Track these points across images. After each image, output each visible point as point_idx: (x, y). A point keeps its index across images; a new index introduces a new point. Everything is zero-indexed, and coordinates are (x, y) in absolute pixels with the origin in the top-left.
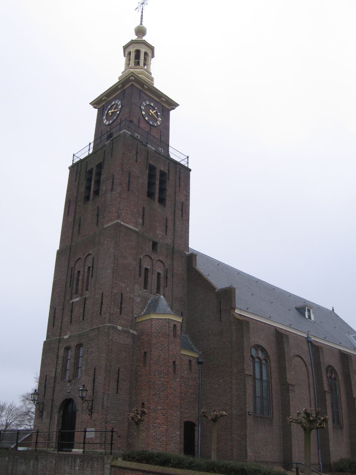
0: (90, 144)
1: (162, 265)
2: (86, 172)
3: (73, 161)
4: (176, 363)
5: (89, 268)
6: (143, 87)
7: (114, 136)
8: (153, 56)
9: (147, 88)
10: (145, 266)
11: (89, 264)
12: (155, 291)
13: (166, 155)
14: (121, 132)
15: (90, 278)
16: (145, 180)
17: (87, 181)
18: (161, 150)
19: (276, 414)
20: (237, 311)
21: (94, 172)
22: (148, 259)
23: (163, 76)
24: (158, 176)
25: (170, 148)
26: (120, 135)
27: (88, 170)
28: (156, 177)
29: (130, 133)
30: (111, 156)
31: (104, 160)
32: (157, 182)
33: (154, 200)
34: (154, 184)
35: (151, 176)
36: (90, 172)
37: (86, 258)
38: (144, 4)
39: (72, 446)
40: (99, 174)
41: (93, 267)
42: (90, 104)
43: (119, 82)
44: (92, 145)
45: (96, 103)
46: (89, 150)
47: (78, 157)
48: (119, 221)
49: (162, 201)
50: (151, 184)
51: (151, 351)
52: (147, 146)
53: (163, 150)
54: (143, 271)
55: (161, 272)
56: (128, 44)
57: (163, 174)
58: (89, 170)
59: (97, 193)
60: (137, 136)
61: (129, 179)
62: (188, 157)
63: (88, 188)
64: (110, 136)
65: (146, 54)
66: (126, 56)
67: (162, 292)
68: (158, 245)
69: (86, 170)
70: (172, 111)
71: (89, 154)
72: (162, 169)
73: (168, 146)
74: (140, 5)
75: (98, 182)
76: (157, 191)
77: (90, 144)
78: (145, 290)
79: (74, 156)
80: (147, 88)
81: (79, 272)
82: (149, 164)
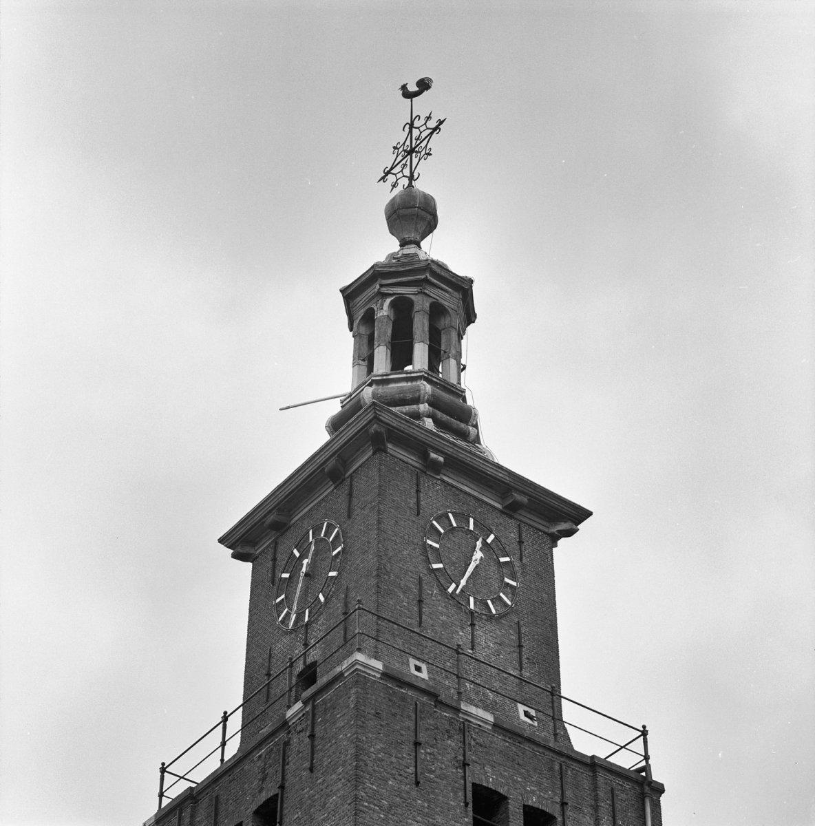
0: (225, 718)
3: (161, 795)
6: (424, 456)
7: (322, 680)
8: (470, 317)
9: (441, 459)
13: (545, 735)
14: (345, 665)
18: (418, 669)
23: (522, 402)
26: (341, 674)
28: (507, 809)
29: (379, 665)
30: (311, 770)
31: (282, 787)
38: (417, 152)
42: (222, 541)
43: (327, 444)
44: (235, 723)
45: (243, 540)
46: (223, 744)
47: (182, 775)
52: (457, 710)
56: (364, 278)
60: (418, 669)
62: (644, 733)
64: (309, 676)
65: (437, 311)
71: (222, 760)
72: (533, 801)
74: (400, 158)
77: (225, 718)
79: (166, 774)
80: (441, 459)
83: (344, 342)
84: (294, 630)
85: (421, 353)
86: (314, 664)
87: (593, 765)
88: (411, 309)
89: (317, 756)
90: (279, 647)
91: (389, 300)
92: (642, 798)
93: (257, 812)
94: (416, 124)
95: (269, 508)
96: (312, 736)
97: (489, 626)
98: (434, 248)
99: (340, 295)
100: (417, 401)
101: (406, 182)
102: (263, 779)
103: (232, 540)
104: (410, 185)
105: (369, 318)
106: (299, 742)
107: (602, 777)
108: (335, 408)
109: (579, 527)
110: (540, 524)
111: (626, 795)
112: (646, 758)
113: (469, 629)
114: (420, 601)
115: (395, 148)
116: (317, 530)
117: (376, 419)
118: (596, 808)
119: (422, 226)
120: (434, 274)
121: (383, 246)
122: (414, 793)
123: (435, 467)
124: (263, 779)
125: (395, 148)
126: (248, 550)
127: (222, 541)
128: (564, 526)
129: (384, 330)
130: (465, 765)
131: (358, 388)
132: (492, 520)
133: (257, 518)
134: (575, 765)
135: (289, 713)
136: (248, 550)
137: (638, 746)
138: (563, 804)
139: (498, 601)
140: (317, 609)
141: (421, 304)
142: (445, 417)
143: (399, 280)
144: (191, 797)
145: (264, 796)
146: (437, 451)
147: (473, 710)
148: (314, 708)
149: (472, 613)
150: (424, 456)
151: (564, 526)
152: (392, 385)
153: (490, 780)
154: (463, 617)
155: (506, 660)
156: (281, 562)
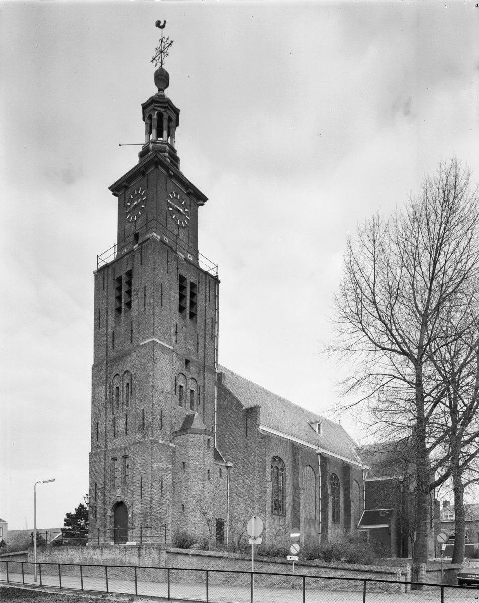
0: (115, 246)
1: (195, 384)
4: (210, 471)
5: (128, 384)
8: (177, 124)
10: (179, 384)
13: (194, 263)
18: (166, 239)
19: (289, 512)
20: (261, 427)
22: (182, 377)
24: (188, 287)
25: (199, 255)
27: (116, 278)
31: (133, 268)
32: (188, 297)
36: (119, 280)
37: (123, 375)
39: (127, 540)
40: (129, 283)
42: (109, 188)
45: (117, 189)
46: (115, 253)
48: (154, 339)
49: (193, 315)
51: (189, 461)
52: (177, 253)
53: (167, 240)
54: (178, 389)
55: (194, 390)
57: (193, 286)
59: (129, 304)
62: (217, 267)
66: (146, 119)
67: (195, 409)
74: (158, 54)
75: (129, 293)
76: (188, 305)
77: (115, 246)
81: (118, 388)
83: (142, 126)
84: (132, 221)
85: (165, 133)
86: (138, 233)
87: (206, 273)
88: (161, 115)
89: (143, 261)
90: (127, 226)
91: (156, 112)
92: (216, 283)
93: (126, 274)
94: (164, 40)
95: (123, 181)
96: (141, 255)
97: (182, 230)
98: (169, 93)
99: (141, 107)
100: (164, 152)
101: (159, 64)
102: (127, 265)
103: (113, 188)
104: (161, 67)
105: (150, 117)
106: (137, 256)
107: (207, 277)
108: (140, 149)
109: (205, 203)
110: (195, 200)
111: (212, 282)
112: (217, 273)
113: (177, 230)
114: (167, 219)
115: (168, 55)
116: (138, 191)
117: (156, 156)
118: (206, 285)
119: (165, 84)
120: (170, 105)
121: (154, 91)
122: (167, 275)
123: (170, 176)
124: (127, 265)
125: (168, 55)
126: (116, 193)
127: (109, 188)
128: (201, 202)
129: (155, 123)
130: (178, 269)
131: (148, 143)
132: (185, 197)
133: (120, 183)
134: (202, 273)
135: (134, 247)
136: (116, 193)
137: (215, 269)
138: (199, 283)
139: (185, 222)
140: (139, 216)
141: (166, 116)
142: (172, 159)
143: (163, 105)
144: (106, 266)
145: (128, 269)
146: (172, 171)
147: (180, 254)
148: (141, 246)
149: (178, 225)
150: (168, 172)
151: (201, 202)
152: (158, 144)
153: (183, 274)
154: (177, 226)
155: (186, 240)
156: (127, 199)
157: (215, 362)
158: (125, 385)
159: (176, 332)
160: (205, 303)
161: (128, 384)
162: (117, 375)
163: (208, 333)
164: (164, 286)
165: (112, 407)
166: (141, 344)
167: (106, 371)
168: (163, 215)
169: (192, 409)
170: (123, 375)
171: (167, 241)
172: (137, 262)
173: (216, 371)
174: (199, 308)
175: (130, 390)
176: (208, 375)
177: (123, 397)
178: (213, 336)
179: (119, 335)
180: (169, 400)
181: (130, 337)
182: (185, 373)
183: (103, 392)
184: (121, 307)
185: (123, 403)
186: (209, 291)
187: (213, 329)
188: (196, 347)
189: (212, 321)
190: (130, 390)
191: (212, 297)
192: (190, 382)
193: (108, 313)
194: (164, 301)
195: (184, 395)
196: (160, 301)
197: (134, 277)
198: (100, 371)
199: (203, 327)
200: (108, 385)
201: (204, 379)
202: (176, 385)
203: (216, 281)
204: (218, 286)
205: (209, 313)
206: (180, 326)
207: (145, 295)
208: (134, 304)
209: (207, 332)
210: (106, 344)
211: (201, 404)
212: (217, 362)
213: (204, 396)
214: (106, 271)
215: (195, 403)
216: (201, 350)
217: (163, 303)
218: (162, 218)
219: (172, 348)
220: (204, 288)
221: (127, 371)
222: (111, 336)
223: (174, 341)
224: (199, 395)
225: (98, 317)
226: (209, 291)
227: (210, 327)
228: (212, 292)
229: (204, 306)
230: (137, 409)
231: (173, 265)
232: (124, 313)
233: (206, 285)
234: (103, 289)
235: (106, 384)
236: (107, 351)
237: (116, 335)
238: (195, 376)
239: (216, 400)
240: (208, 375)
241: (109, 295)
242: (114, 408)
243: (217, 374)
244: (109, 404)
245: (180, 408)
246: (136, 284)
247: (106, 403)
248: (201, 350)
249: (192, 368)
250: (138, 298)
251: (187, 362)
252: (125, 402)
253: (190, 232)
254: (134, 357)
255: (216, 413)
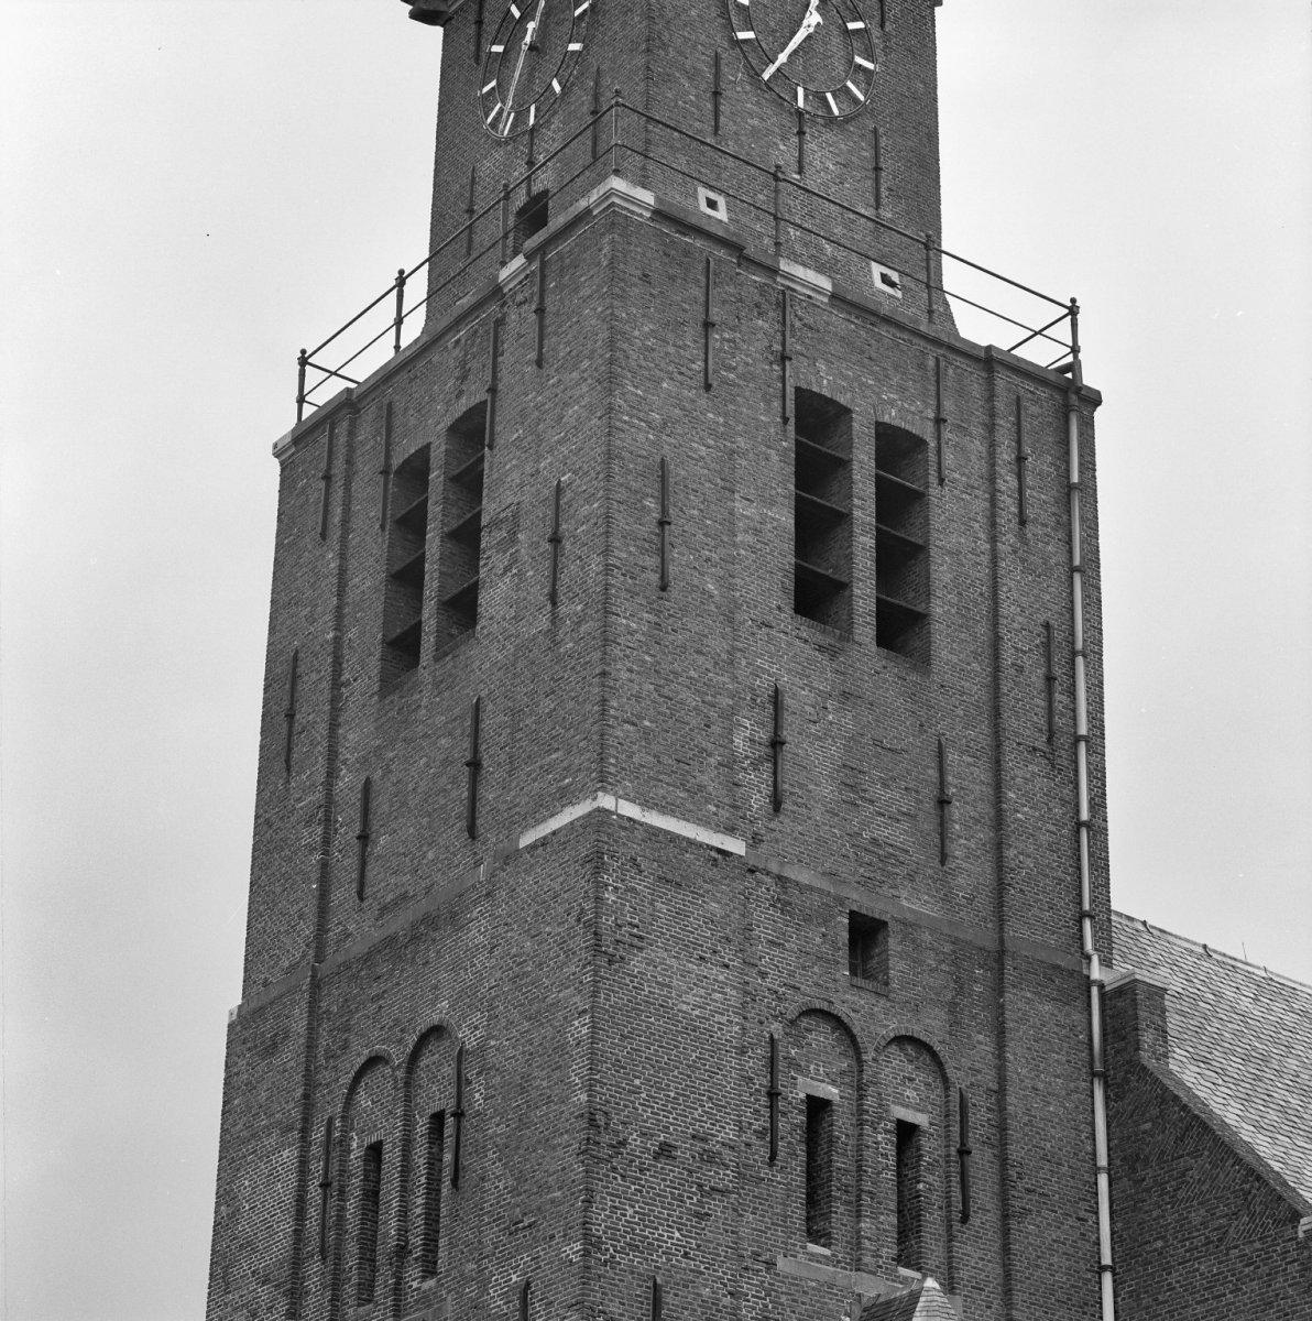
0: (401, 281)
2: (385, 472)
3: (301, 400)
5: (438, 1118)
7: (557, 221)
10: (804, 1087)
11: (435, 1096)
12: (889, 1251)
13: (913, 313)
15: (446, 1190)
16: (767, 515)
17: (395, 521)
21: (436, 476)
22: (821, 1036)
24: (863, 461)
26: (588, 211)
27: (396, 462)
29: (647, 197)
30: (539, 363)
31: (493, 390)
32: (864, 511)
33: (847, 634)
34: (842, 519)
35: (816, 468)
36: (415, 471)
37: (414, 1057)
40: (469, 483)
41: (459, 1115)
44: (417, 288)
46: (399, 321)
47: (333, 370)
48: (606, 801)
49: (900, 628)
50: (816, 526)
52: (773, 271)
54: (793, 1121)
55: (920, 1119)
57: (896, 447)
58: (407, 462)
59: (463, 608)
61: (664, 511)
62: (1073, 311)
63: (407, 578)
68: (893, 944)
69: (388, 456)
70: (1112, 904)
71: (397, 347)
73: (931, 246)
75: (467, 537)
77: (401, 281)
78: (813, 1248)
79: (308, 367)
81: (375, 1152)
82: (798, 389)
84: (512, 139)
87: (989, 361)
96: (540, 311)
97: (828, 136)
106: (520, 320)
111: (1039, 408)
112: (1075, 350)
114: (716, 94)
118: (991, 428)
122: (703, 402)
124: (463, 378)
130: (784, 358)
135: (504, 274)
137: (1063, 331)
139: (843, 94)
144: (349, 405)
147: (799, 271)
148: (543, 265)
149: (800, 113)
153: (825, 382)
154: (787, 121)
155: (855, 191)
157: (1082, 915)
158: (422, 1126)
159: (776, 744)
160: (993, 540)
161: (438, 1118)
162: (374, 1061)
163: (1024, 723)
164: (677, 472)
165: (336, 1286)
166: (527, 840)
167: (311, 1046)
168: (693, 75)
169: (904, 1259)
170: (414, 1057)
171: (722, 214)
172: (516, 356)
173: (1096, 972)
174: (942, 571)
175: (448, 1157)
176: (1029, 1008)
177: (404, 1214)
178: (1063, 740)
179: (404, 804)
180: (715, 1205)
181: (461, 809)
182: (840, 1009)
183: (285, 1189)
184: (417, 629)
185: (402, 1251)
186: (1020, 459)
187: (1060, 697)
188: (929, 825)
189: (1047, 645)
190: (448, 1157)
191: (1041, 499)
192: (893, 1068)
193: (346, 676)
194: (679, 558)
195: (839, 1162)
196: (652, 561)
197: (500, 442)
198: (271, 1049)
199: (977, 690)
200: (318, 1135)
201: (1000, 1034)
202: (773, 1095)
203: (1069, 398)
204: (1088, 426)
205: (1022, 604)
206: (800, 699)
207: (556, 540)
208: (494, 599)
209: (1010, 722)
210: (324, 865)
211: (985, 1216)
212: (1101, 911)
213: (1003, 1160)
214: (342, 429)
215: (933, 1220)
216: (968, 842)
217: (672, 569)
218: (685, 98)
219: (736, 846)
220: (977, 446)
221: (437, 1031)
222: (355, 813)
223: (758, 801)
224: (964, 1152)
225: (286, 704)
226: (1020, 459)
227: (1037, 678)
228: (1040, 464)
229: (985, 559)
230: (484, 1286)
231: (747, 346)
232: (437, 659)
233: (991, 428)
234: (323, 536)
235: (305, 1132)
236: (323, 911)
237: (381, 805)
238: (932, 1026)
239: (1103, 1180)
240: (1029, 1008)
241: (353, 564)
242: (350, 1290)
243: (1102, 996)
244: (314, 1271)
245: (808, 1263)
246: (511, 482)
247: (297, 1262)
248: (968, 842)
249: (897, 968)
250: (514, 560)
251: (865, 934)
252: (416, 1240)
253: (883, 142)
254: (476, 934)
255: (1107, 1279)
